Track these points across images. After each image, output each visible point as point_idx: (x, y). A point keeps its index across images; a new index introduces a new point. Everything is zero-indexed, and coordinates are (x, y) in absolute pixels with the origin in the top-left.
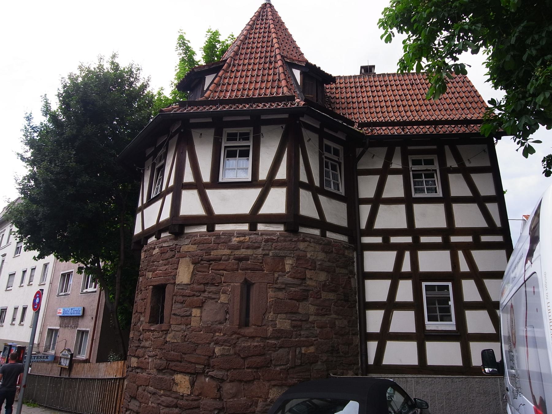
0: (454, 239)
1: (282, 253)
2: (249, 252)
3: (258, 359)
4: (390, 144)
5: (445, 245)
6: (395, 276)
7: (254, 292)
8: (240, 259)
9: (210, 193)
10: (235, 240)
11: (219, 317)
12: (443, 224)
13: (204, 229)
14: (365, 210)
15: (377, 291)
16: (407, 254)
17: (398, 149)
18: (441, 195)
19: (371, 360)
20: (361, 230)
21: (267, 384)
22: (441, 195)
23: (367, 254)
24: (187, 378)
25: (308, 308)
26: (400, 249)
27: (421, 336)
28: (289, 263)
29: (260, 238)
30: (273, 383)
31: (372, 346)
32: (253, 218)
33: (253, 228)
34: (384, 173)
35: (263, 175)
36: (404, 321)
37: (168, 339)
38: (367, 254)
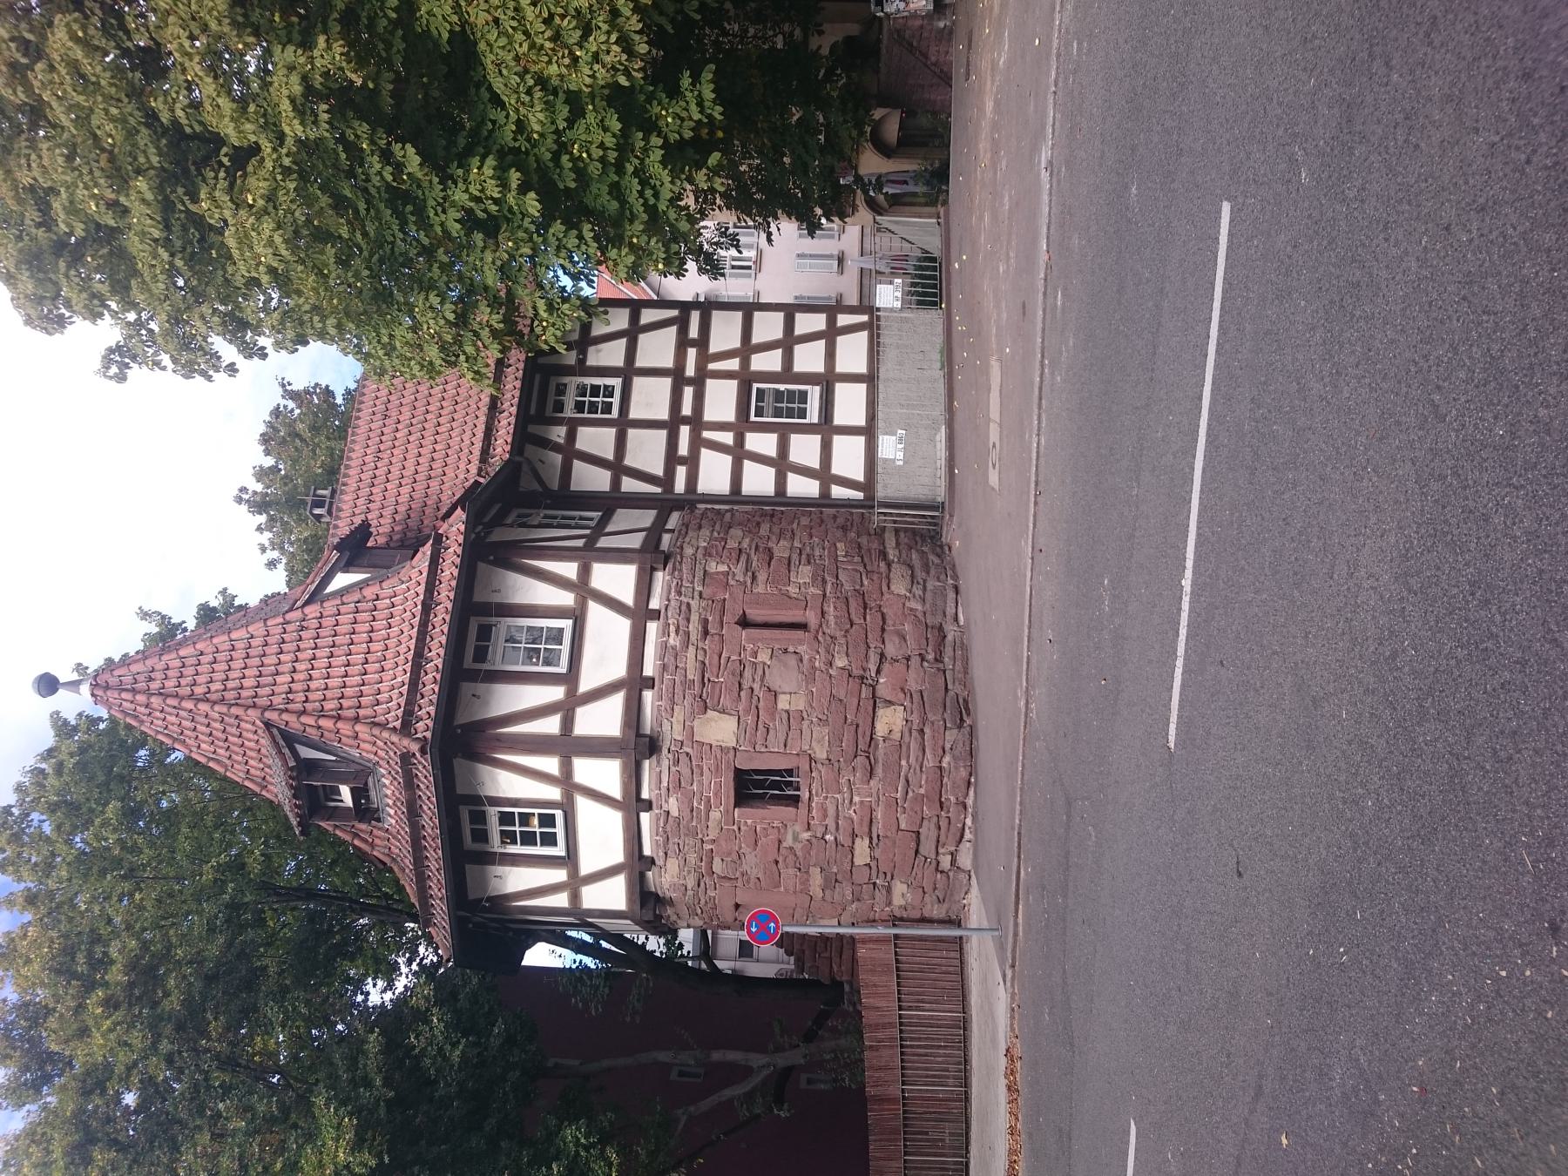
0: (690, 371)
1: (699, 574)
2: (694, 617)
3: (853, 604)
4: (524, 437)
5: (699, 383)
6: (739, 454)
7: (755, 614)
8: (706, 633)
9: (585, 686)
10: (673, 640)
11: (792, 661)
12: (667, 382)
13: (648, 696)
14: (629, 485)
15: (758, 480)
16: (706, 434)
17: (532, 429)
18: (620, 380)
19: (859, 495)
20: (665, 492)
21: (886, 596)
22: (620, 380)
23: (703, 486)
24: (880, 712)
25: (781, 549)
26: (697, 443)
27: (827, 428)
28: (713, 567)
29: (673, 603)
30: (885, 588)
31: (837, 492)
32: (640, 614)
33: (655, 615)
34: (570, 452)
35: (566, 599)
36: (805, 449)
37: (825, 756)
38: (703, 486)
